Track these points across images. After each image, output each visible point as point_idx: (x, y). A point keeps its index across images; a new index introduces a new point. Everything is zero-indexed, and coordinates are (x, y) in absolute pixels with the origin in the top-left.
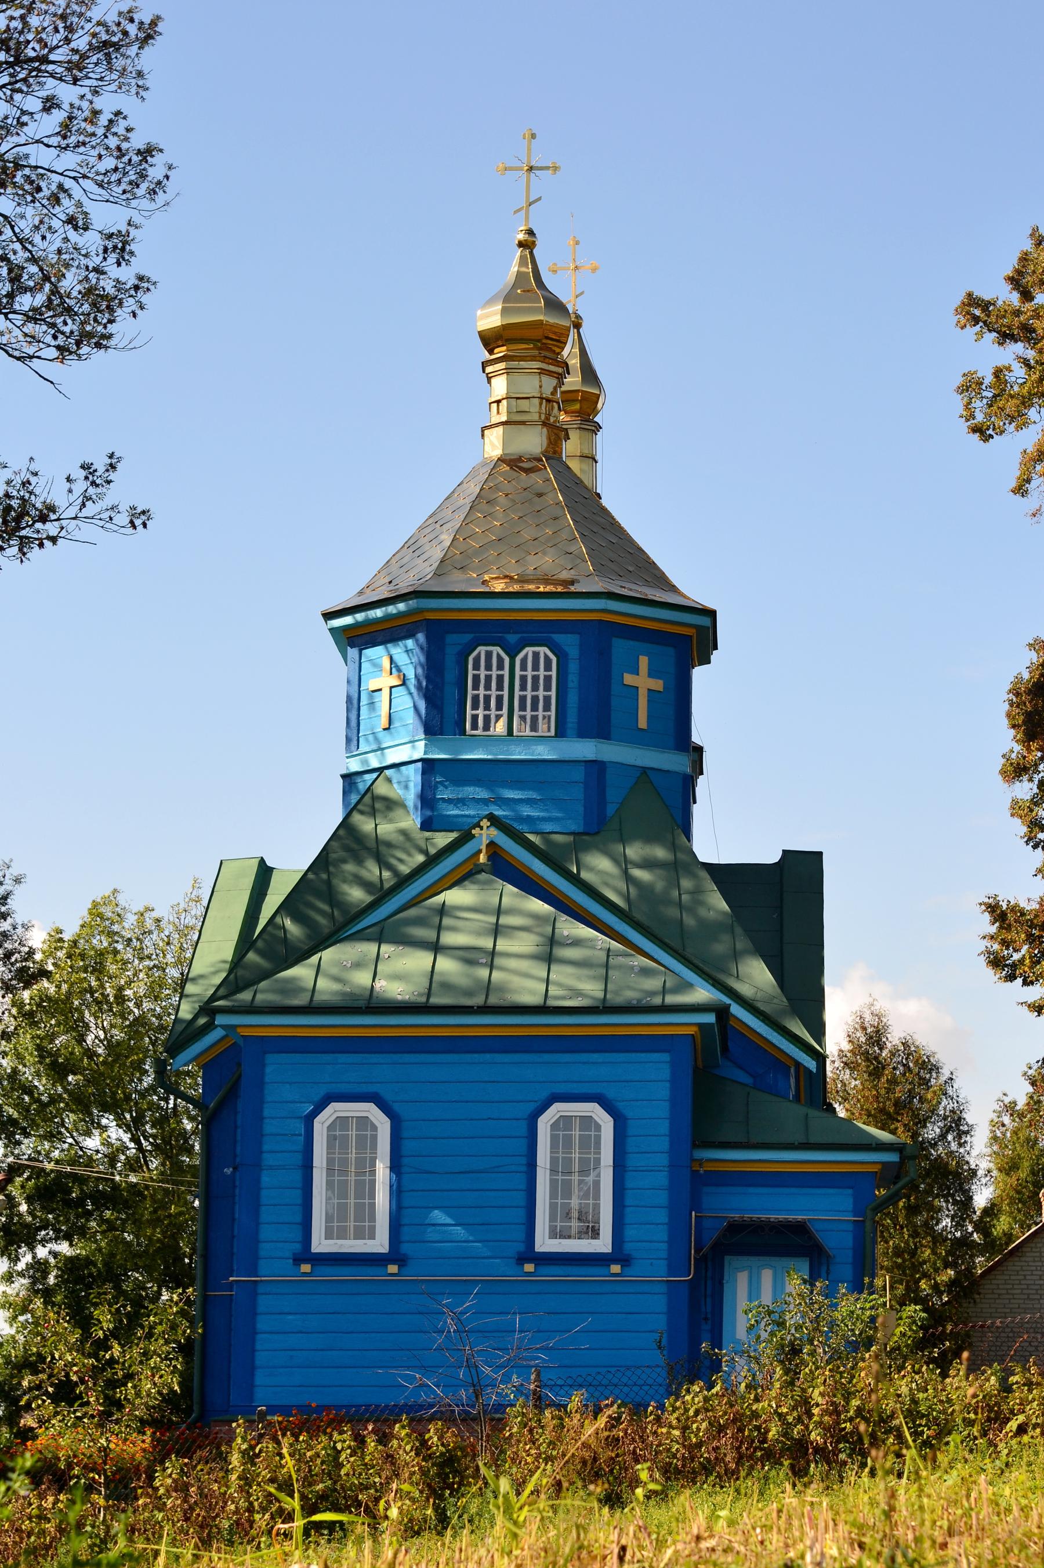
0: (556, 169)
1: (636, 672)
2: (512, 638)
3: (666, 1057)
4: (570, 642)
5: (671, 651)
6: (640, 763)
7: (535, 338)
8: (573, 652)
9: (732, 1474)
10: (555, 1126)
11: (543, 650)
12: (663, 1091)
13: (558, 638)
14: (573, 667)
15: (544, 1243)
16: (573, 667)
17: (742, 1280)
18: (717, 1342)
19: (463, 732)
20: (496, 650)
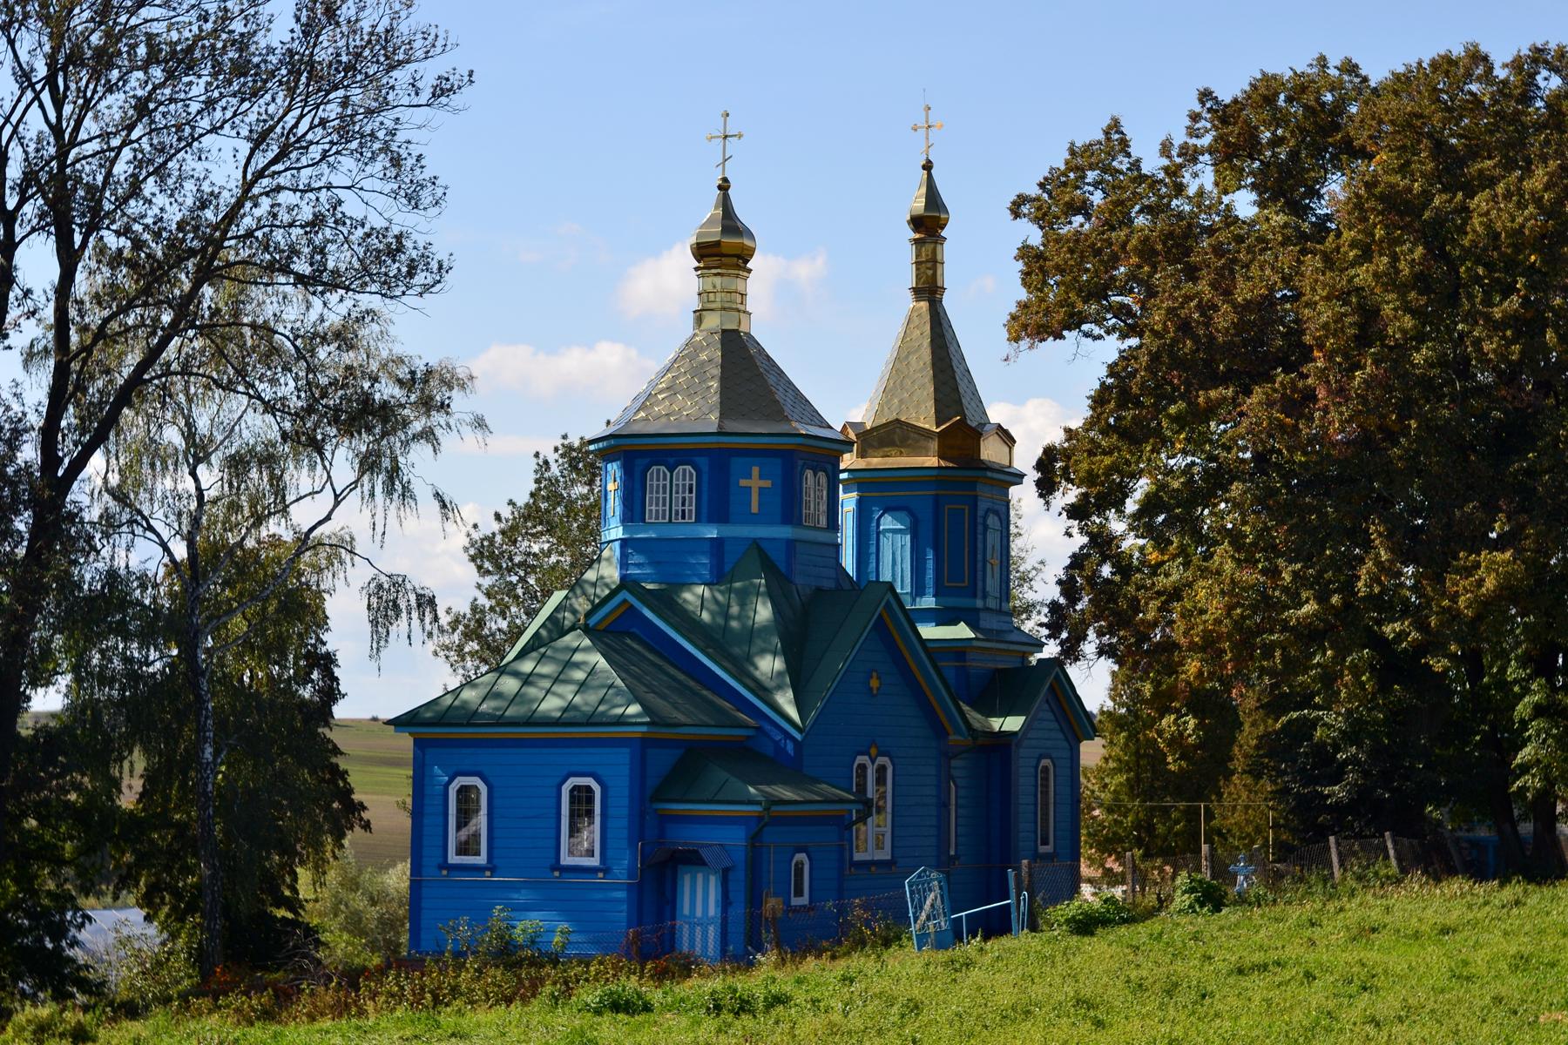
0: (740, 136)
1: (749, 476)
2: (671, 460)
3: (626, 750)
4: (703, 462)
5: (778, 461)
6: (752, 535)
7: (928, 166)
8: (705, 469)
9: (1399, 881)
10: (572, 791)
11: (688, 468)
12: (626, 770)
13: (698, 459)
14: (705, 478)
15: (566, 860)
16: (705, 478)
17: (687, 879)
18: (673, 918)
19: (643, 520)
20: (663, 468)
